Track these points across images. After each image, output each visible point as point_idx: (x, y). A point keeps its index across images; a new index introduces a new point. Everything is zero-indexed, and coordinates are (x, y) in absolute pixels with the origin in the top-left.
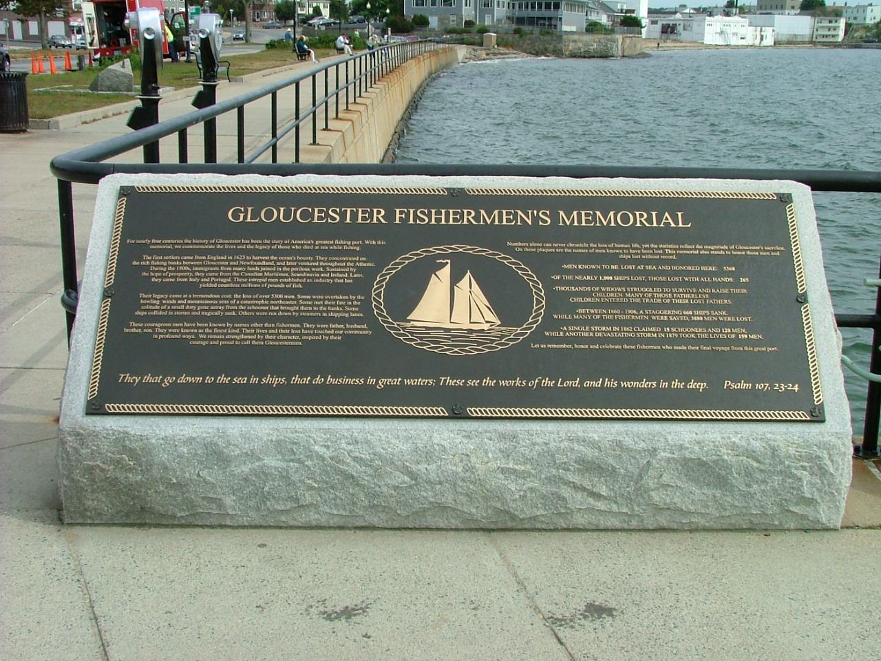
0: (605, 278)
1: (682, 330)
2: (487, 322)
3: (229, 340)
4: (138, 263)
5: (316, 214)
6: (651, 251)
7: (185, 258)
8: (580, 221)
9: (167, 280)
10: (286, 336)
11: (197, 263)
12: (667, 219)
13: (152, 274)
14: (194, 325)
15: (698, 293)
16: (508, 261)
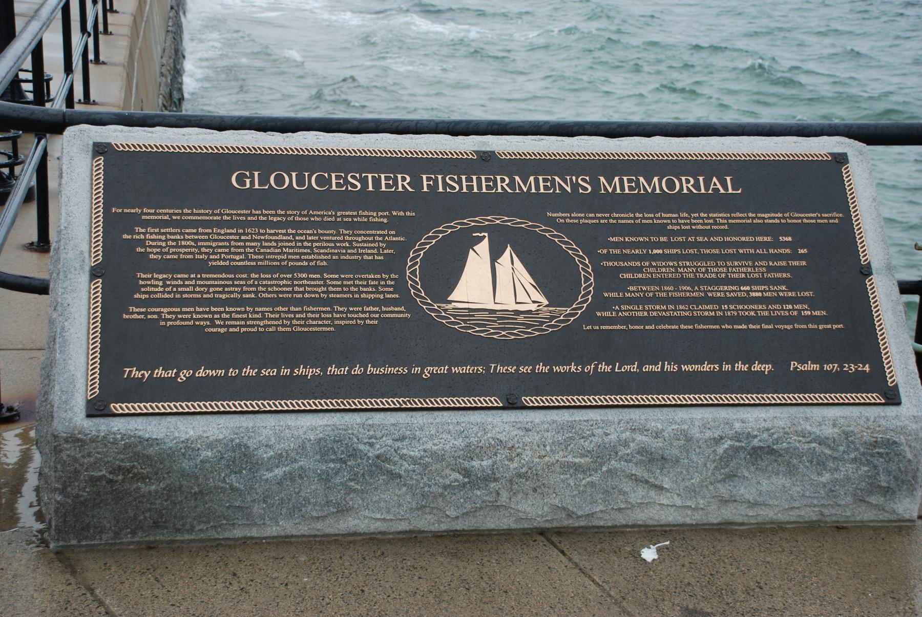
0: (655, 251)
1: (741, 307)
2: (534, 302)
3: (250, 326)
4: (129, 237)
5: (334, 181)
6: (701, 221)
7: (187, 231)
8: (622, 188)
9: (168, 257)
10: (317, 321)
11: (203, 237)
12: (715, 185)
13: (148, 250)
14: (207, 309)
15: (754, 267)
16: (550, 234)
